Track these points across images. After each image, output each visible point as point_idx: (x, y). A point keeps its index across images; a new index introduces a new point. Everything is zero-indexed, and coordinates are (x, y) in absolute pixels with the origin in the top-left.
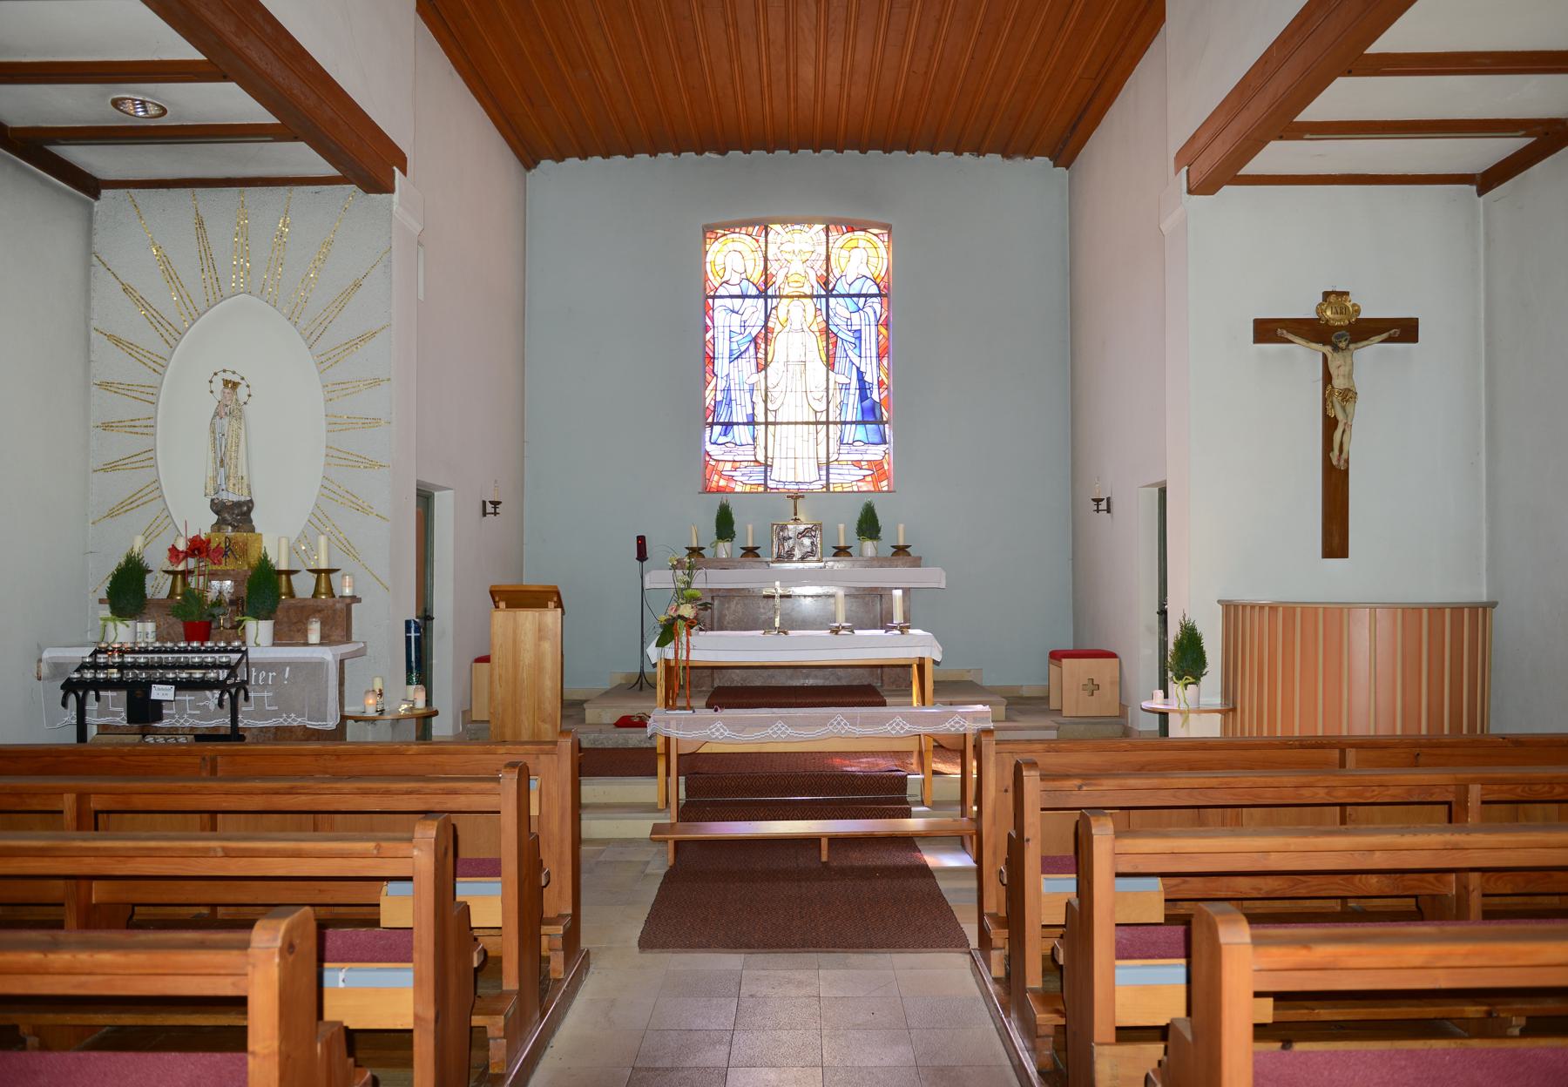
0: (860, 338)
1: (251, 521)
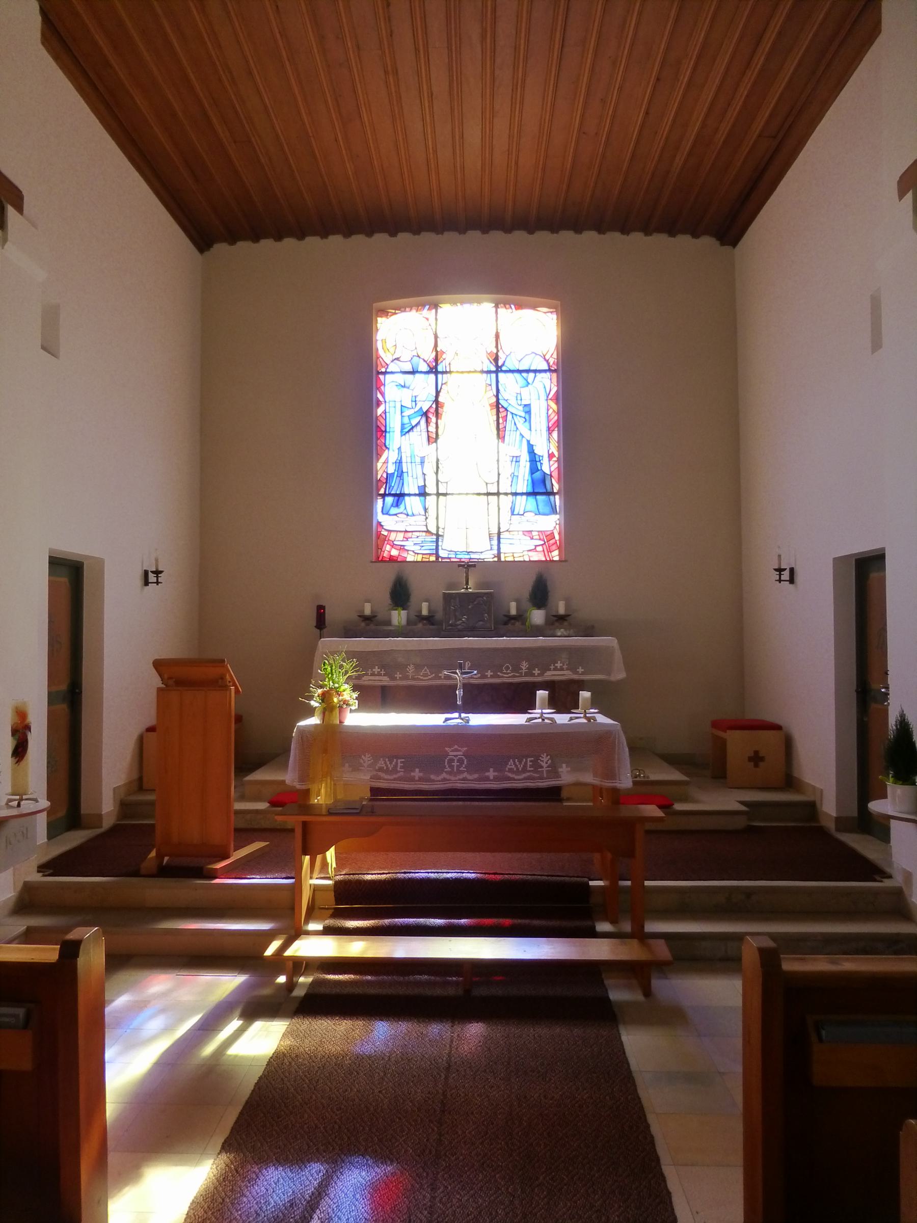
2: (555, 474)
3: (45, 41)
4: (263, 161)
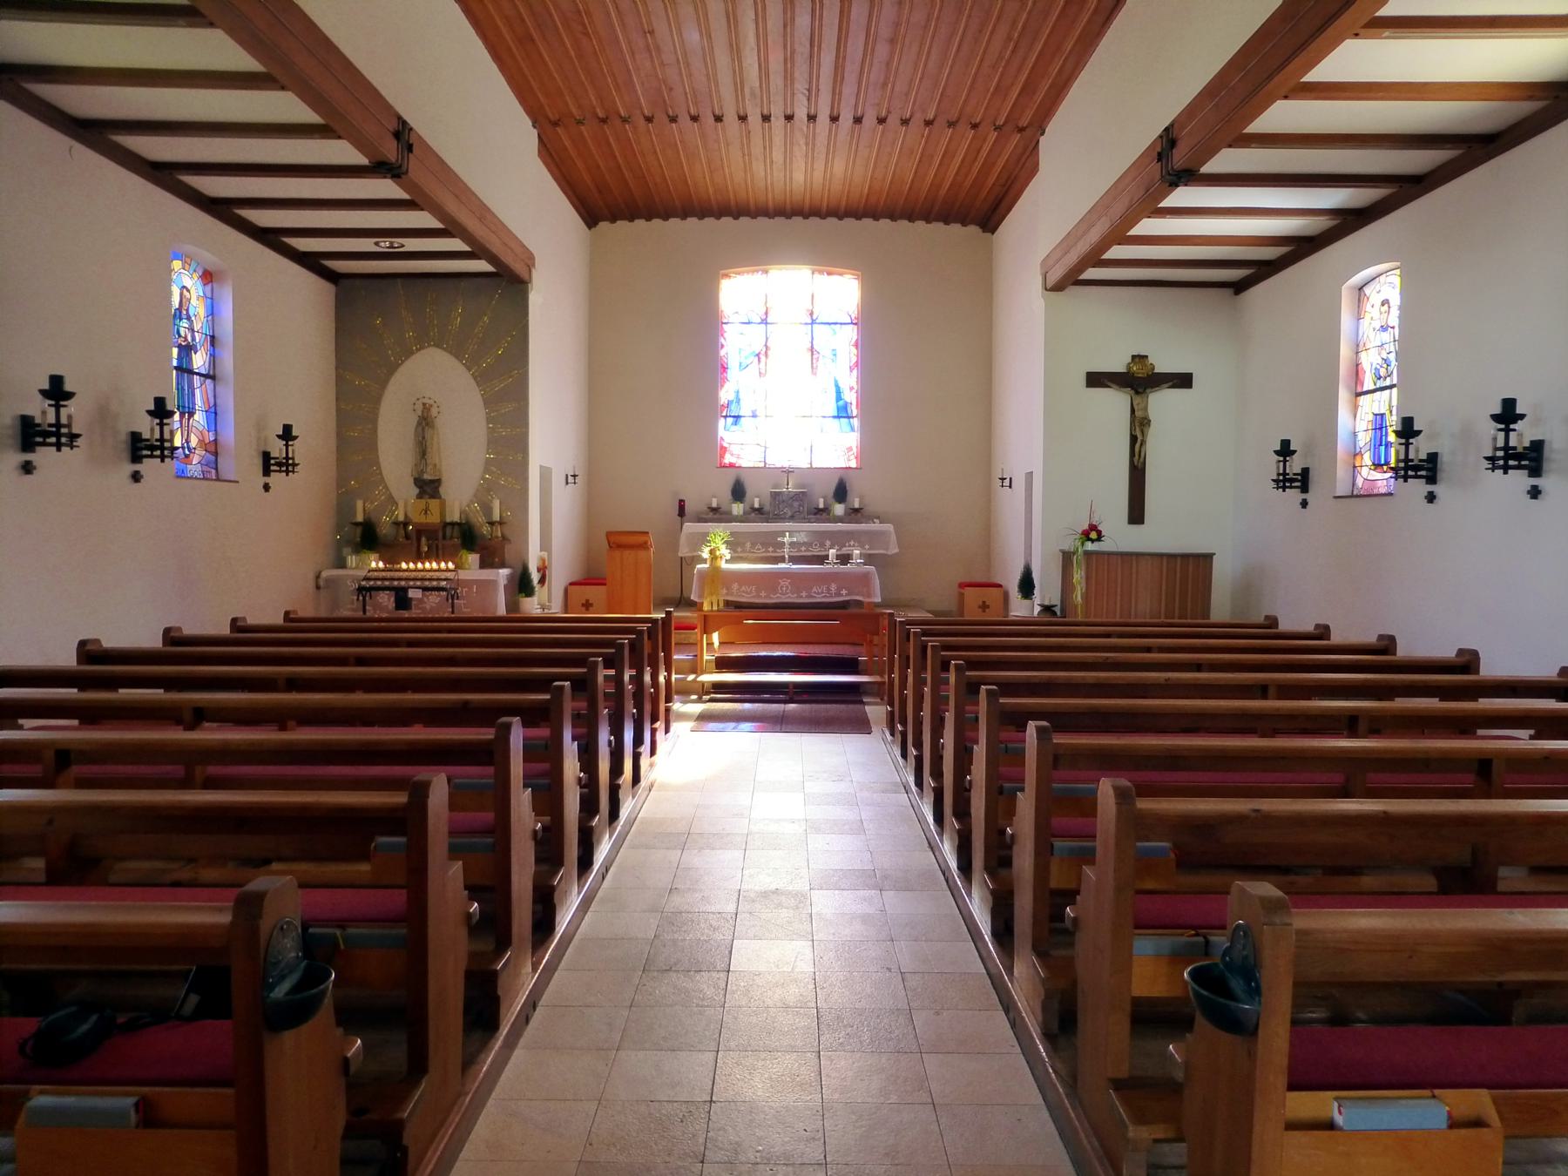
3: (540, 154)
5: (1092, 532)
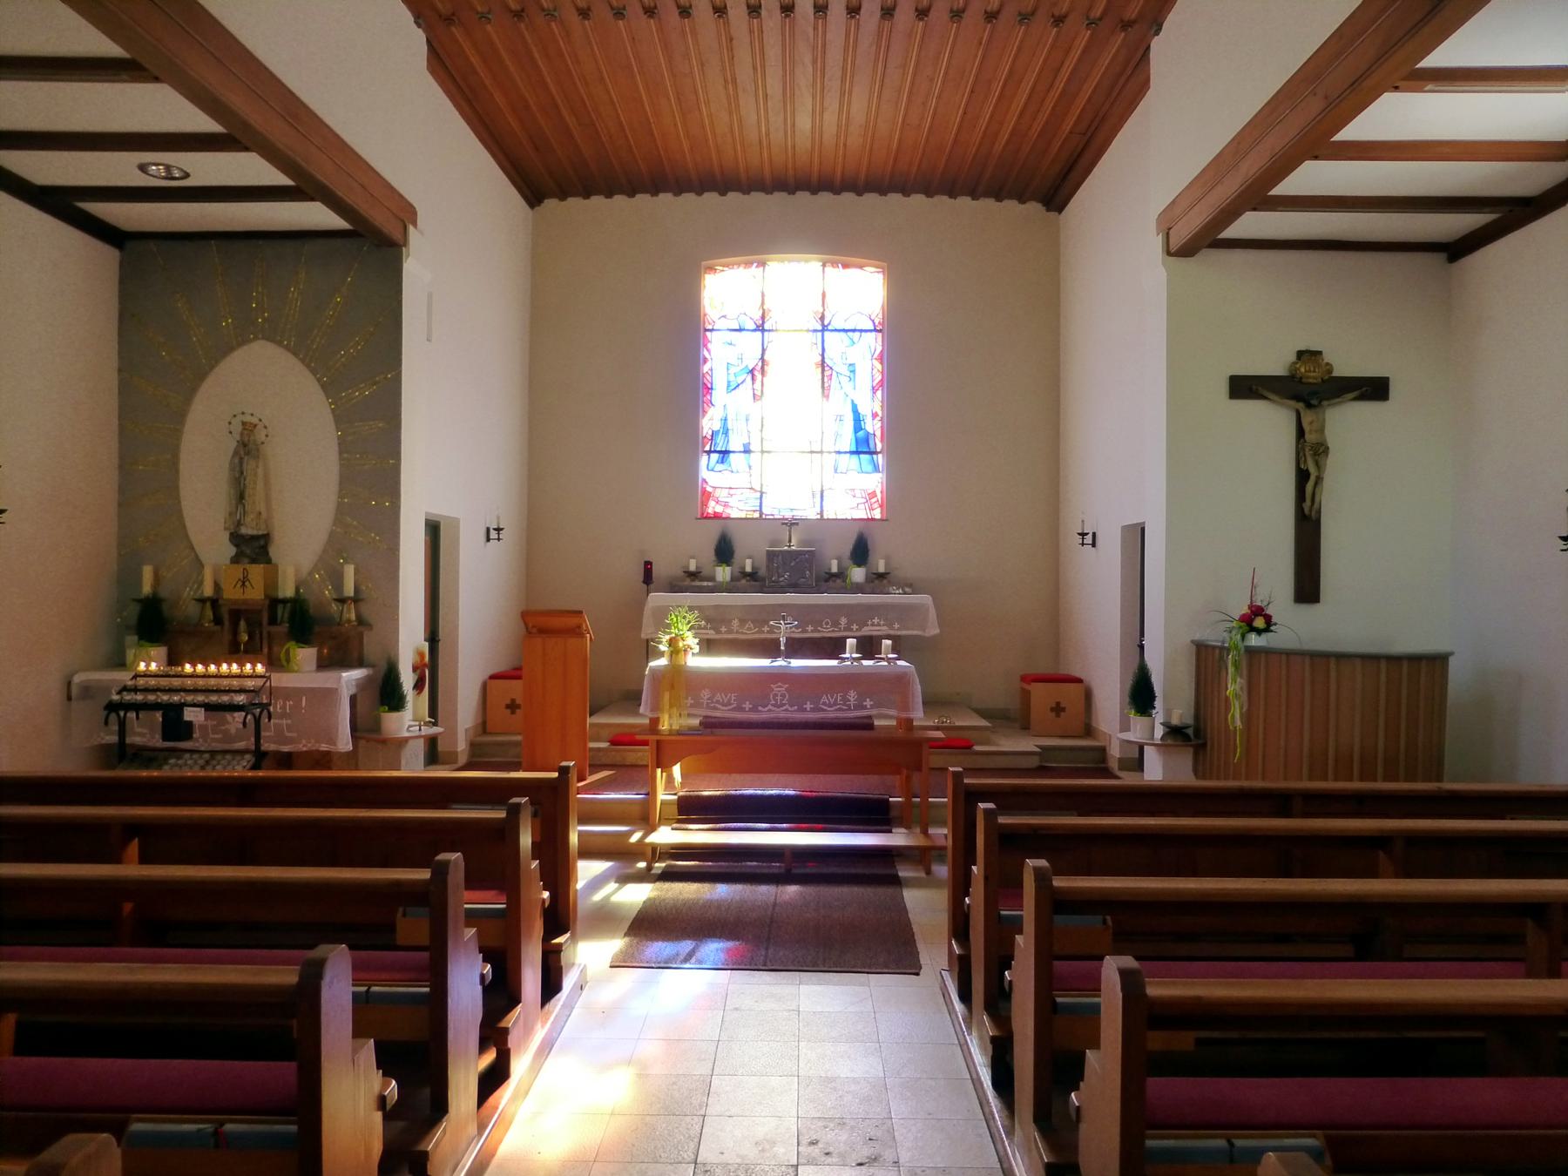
0: (853, 372)
1: (267, 553)
2: (878, 434)
4: (604, 139)
5: (1256, 618)
